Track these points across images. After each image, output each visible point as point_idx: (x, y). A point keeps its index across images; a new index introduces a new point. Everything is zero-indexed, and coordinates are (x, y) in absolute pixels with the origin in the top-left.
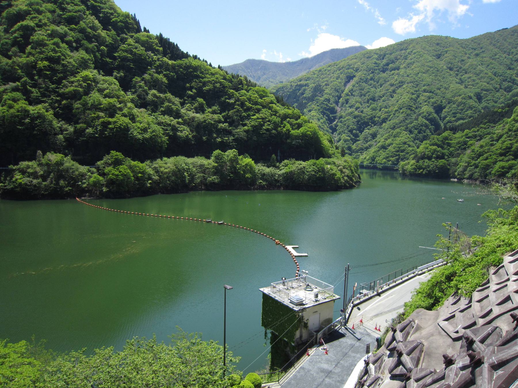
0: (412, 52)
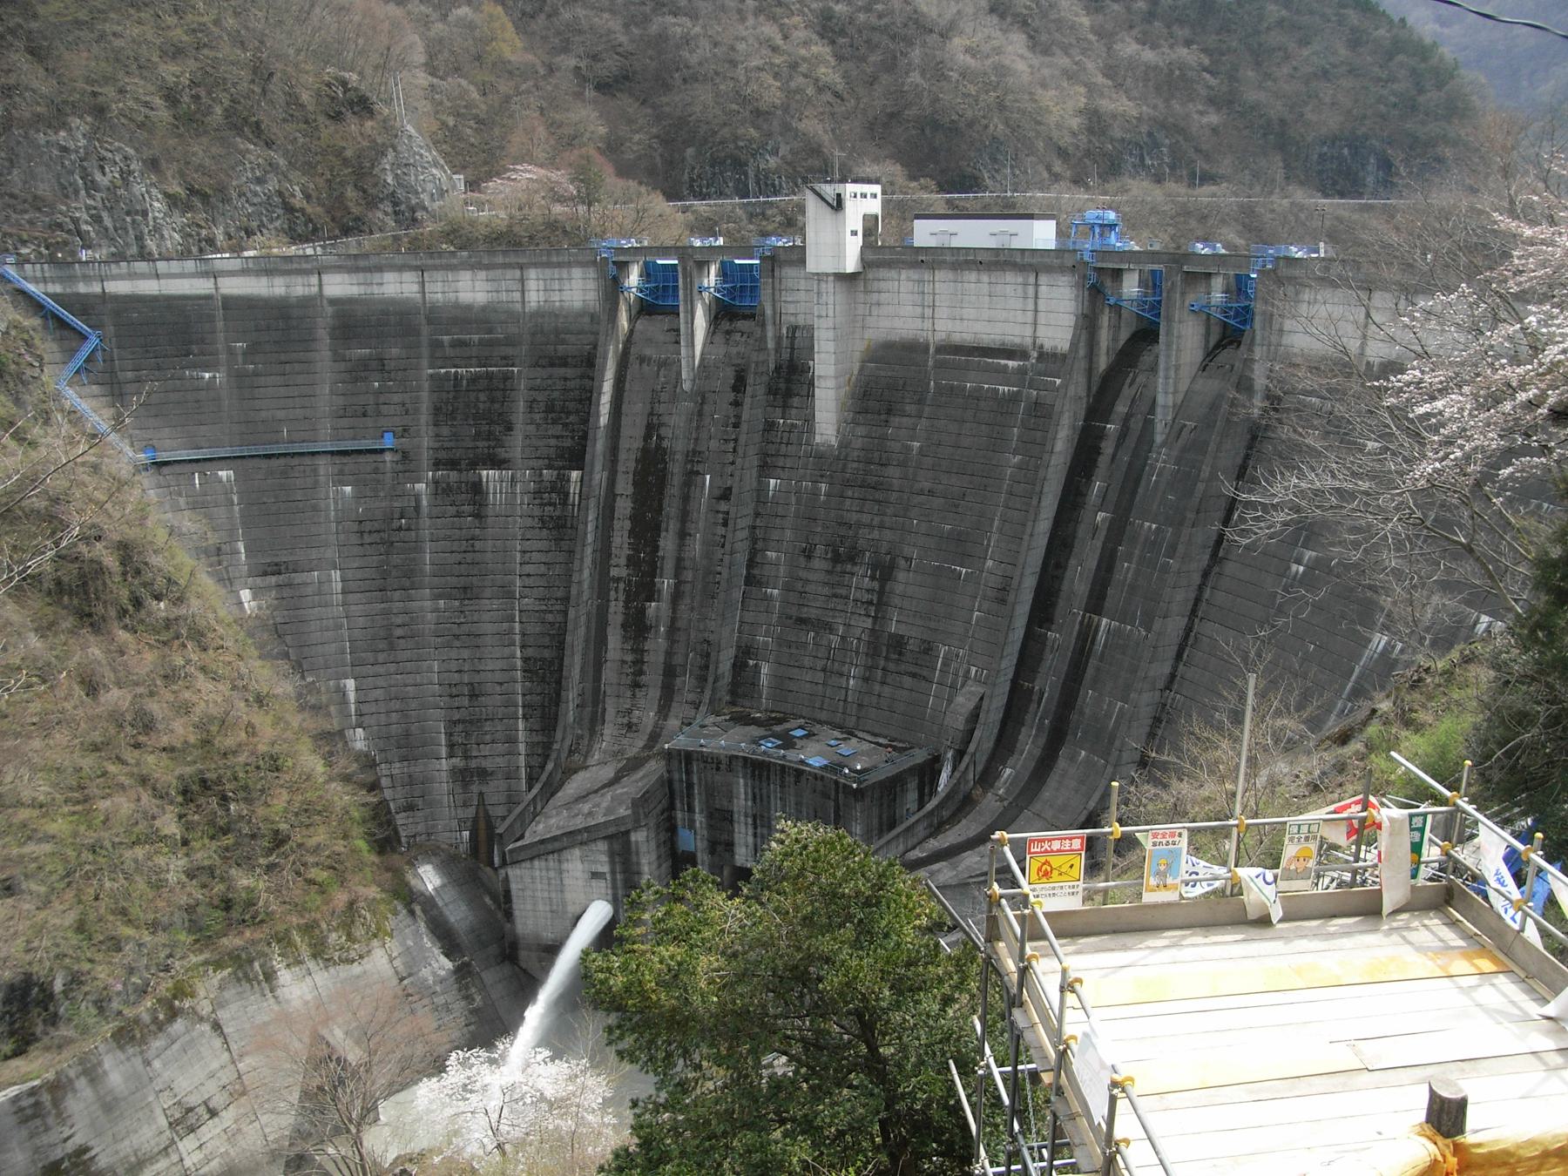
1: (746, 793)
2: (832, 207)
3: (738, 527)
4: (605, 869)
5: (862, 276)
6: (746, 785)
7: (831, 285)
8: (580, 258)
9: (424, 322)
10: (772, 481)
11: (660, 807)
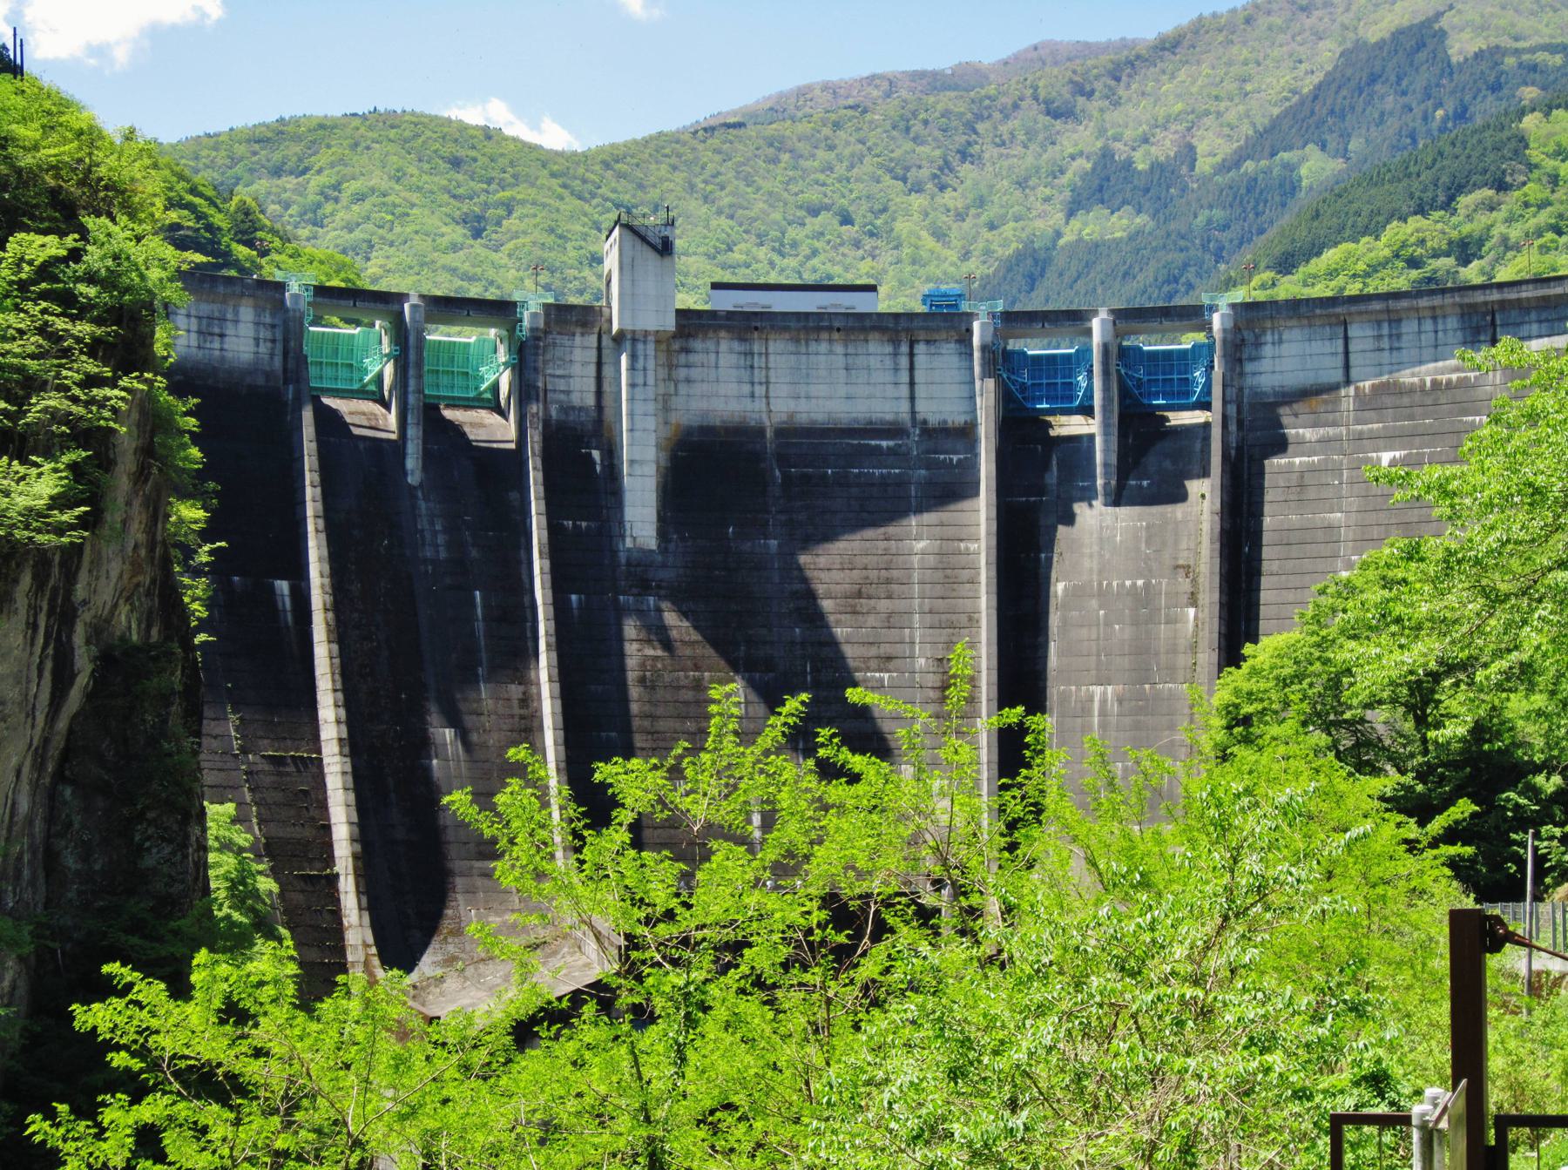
0: (337, 187)
9: (342, 257)
10: (574, 597)
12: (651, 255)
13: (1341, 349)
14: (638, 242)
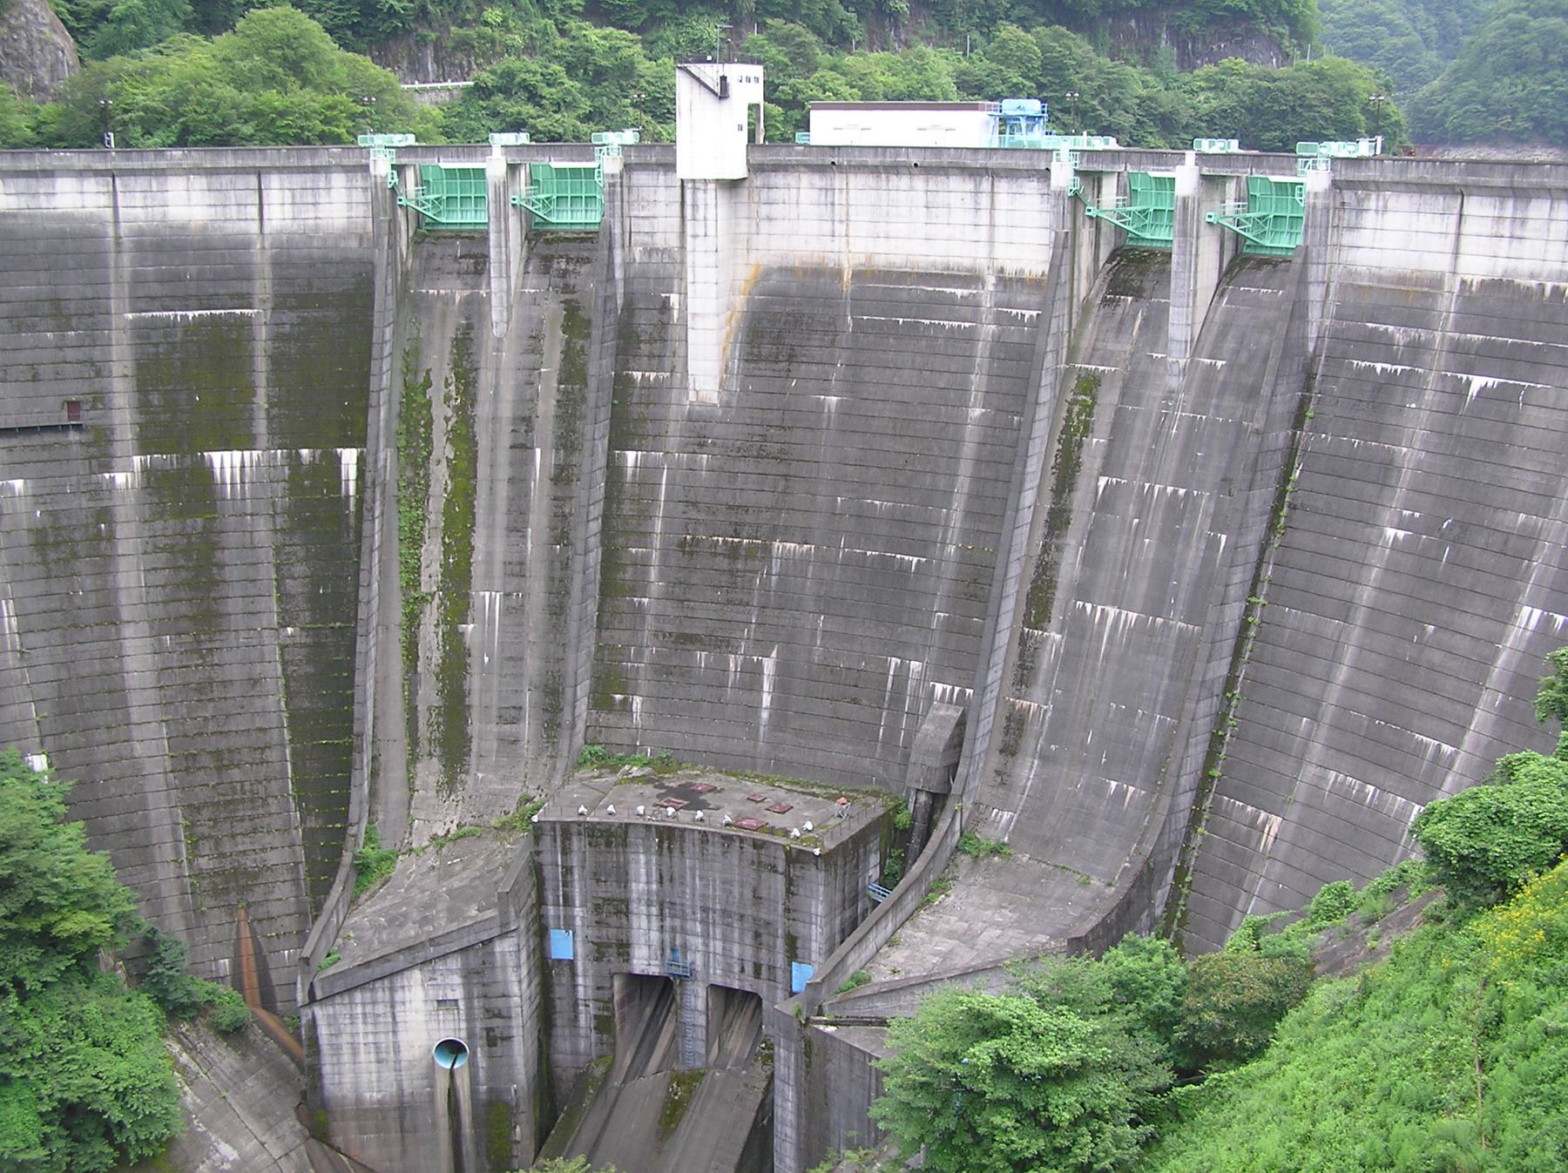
1: (648, 874)
2: (716, 94)
3: (591, 517)
4: (458, 994)
5: (746, 184)
6: (648, 863)
7: (711, 194)
8: (345, 162)
11: (529, 903)
12: (709, 100)
13: (1453, 229)
14: (696, 85)
